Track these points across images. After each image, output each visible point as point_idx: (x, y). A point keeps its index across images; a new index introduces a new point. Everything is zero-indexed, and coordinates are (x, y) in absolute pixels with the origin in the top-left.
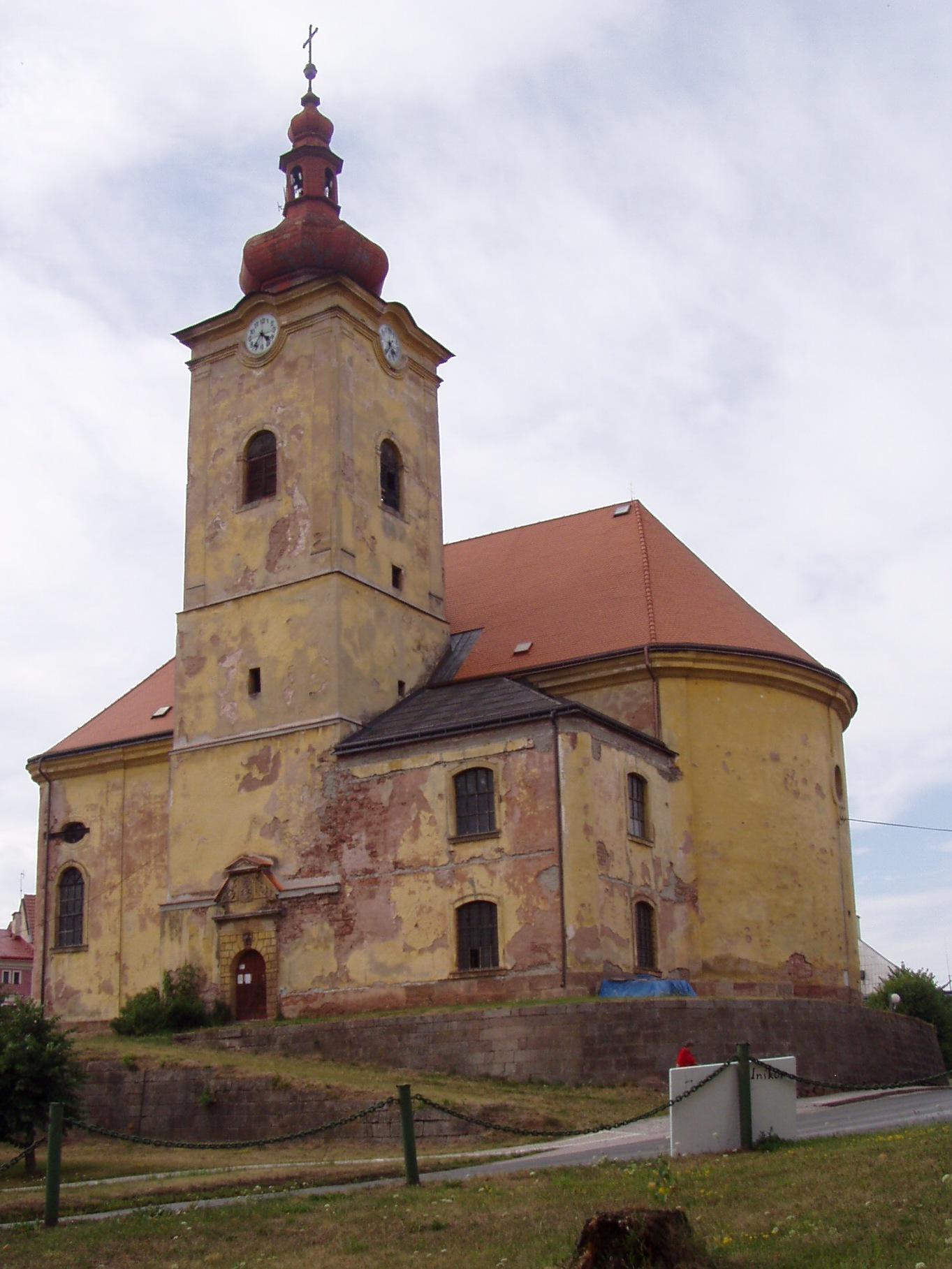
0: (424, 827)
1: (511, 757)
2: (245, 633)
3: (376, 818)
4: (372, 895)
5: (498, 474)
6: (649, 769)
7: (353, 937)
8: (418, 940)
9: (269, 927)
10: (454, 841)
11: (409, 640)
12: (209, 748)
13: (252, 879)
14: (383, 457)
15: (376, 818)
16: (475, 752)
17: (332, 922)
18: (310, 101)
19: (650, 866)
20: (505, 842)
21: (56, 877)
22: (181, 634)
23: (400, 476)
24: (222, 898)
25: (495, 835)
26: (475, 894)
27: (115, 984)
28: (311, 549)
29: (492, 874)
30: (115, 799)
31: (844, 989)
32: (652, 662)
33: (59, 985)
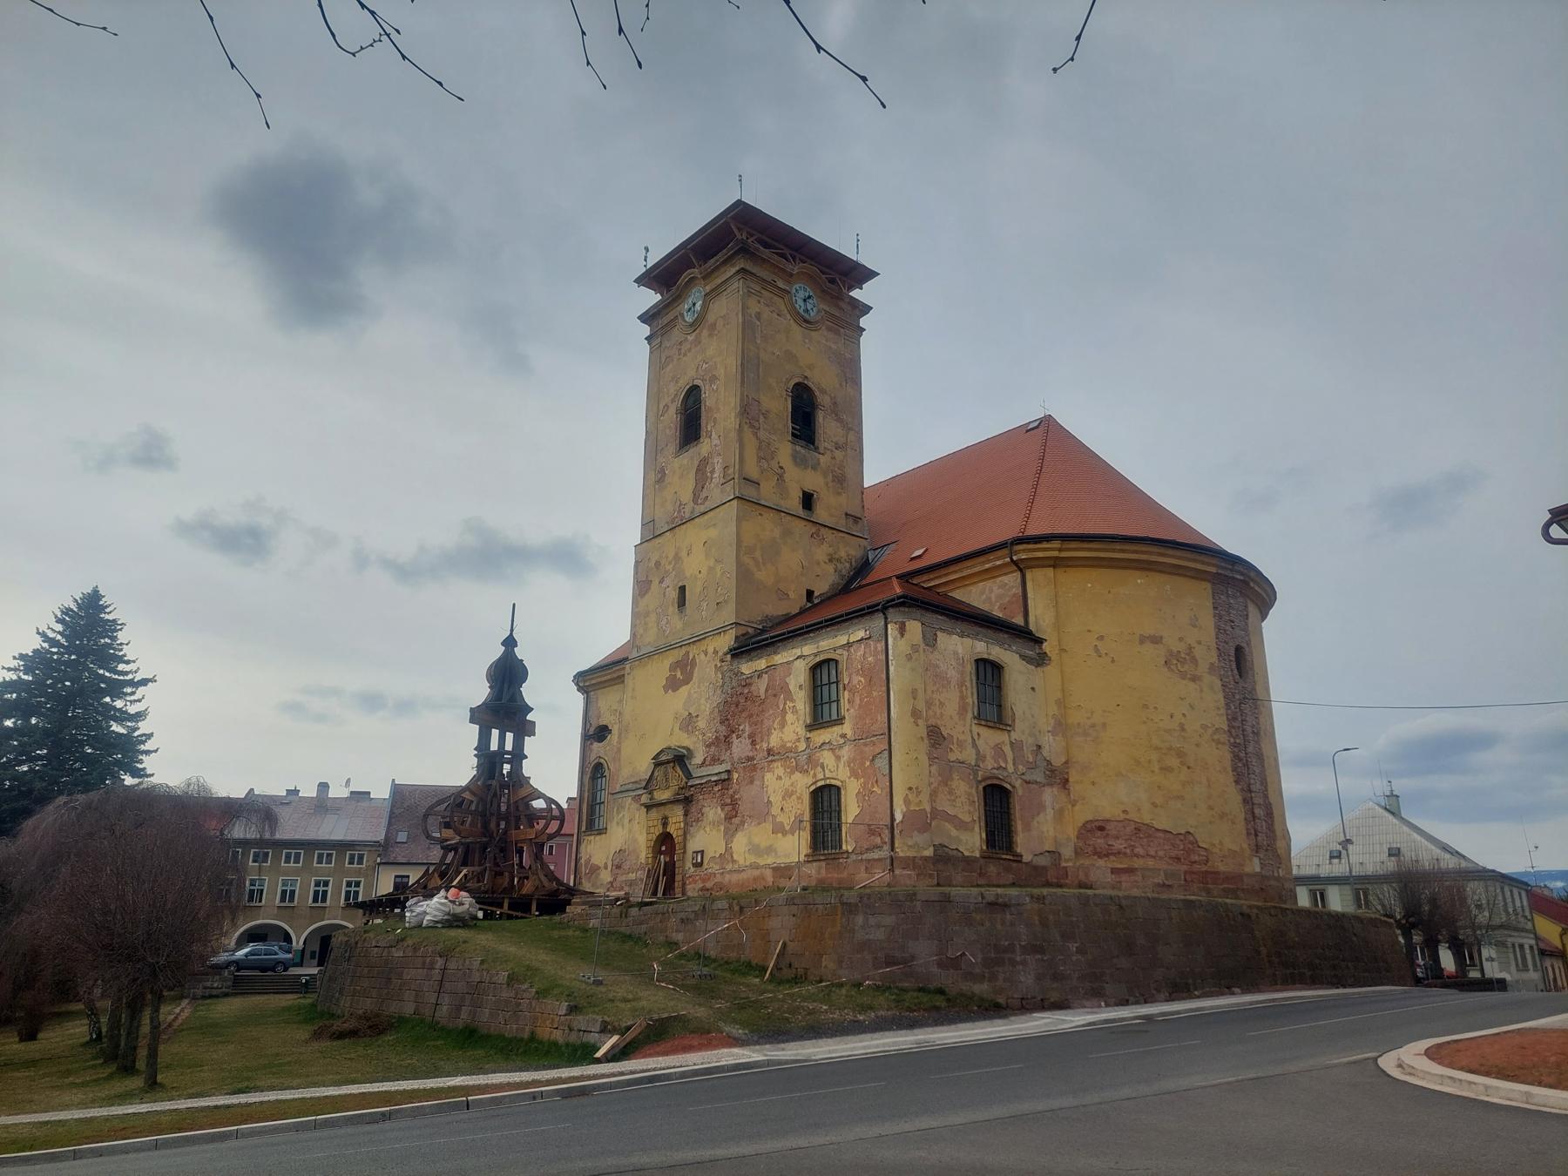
0: (790, 717)
4: (752, 782)
5: (912, 416)
6: (1008, 656)
7: (736, 821)
8: (786, 820)
10: (811, 727)
11: (821, 553)
12: (650, 655)
17: (723, 805)
19: (1007, 749)
20: (847, 728)
21: (589, 770)
22: (637, 563)
24: (649, 785)
25: (840, 721)
26: (825, 779)
29: (838, 758)
31: (1256, 875)
32: (1019, 552)
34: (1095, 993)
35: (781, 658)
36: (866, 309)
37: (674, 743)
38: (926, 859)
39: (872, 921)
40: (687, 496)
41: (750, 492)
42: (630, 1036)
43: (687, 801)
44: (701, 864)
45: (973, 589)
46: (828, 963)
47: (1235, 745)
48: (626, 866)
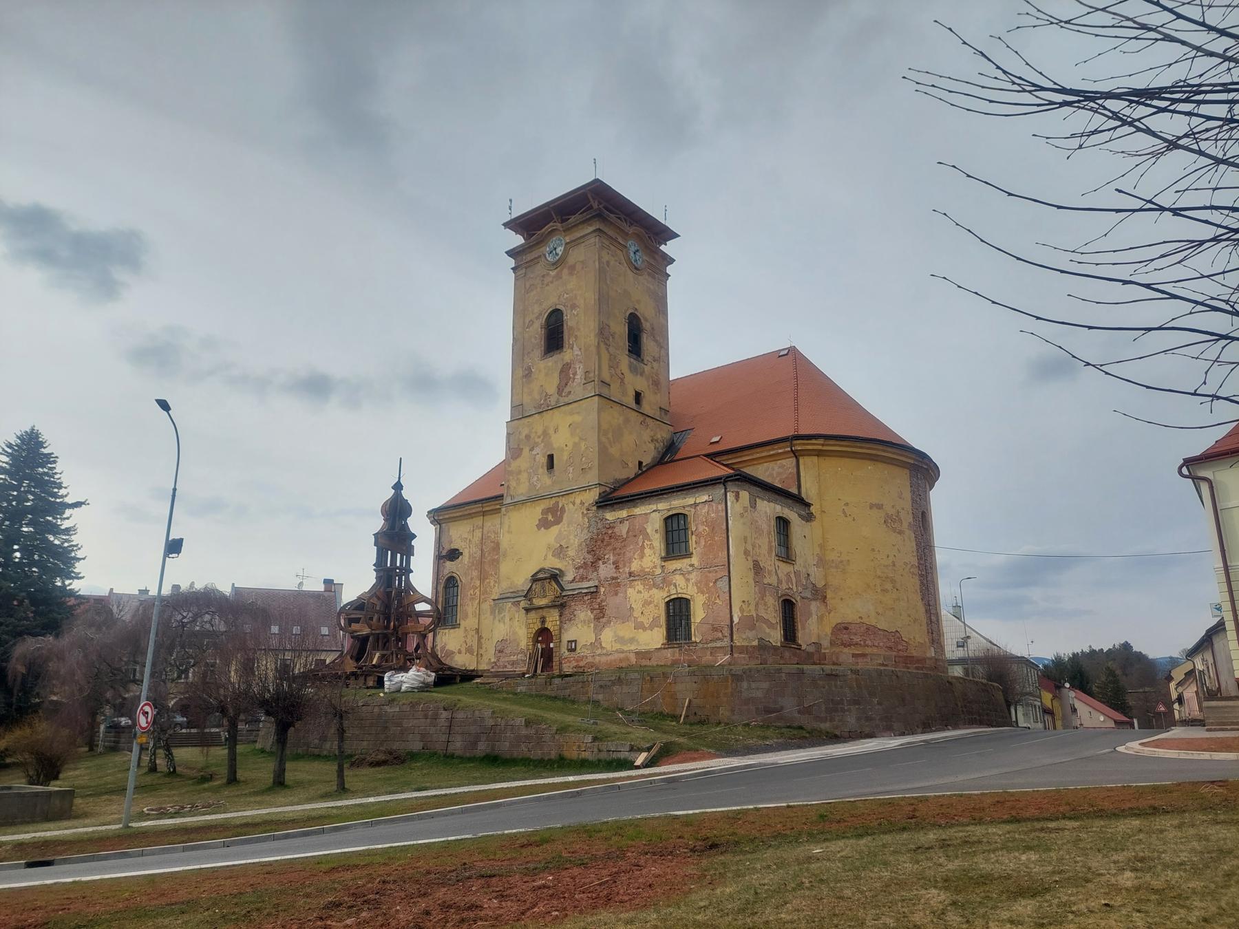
0: (647, 551)
1: (699, 507)
3: (618, 545)
5: (703, 336)
6: (791, 515)
7: (604, 620)
8: (646, 621)
10: (665, 559)
11: (646, 435)
12: (523, 502)
13: (546, 583)
14: (630, 323)
15: (618, 545)
16: (677, 503)
17: (592, 610)
19: (792, 576)
20: (695, 560)
21: (442, 582)
23: (639, 336)
24: (528, 595)
25: (689, 555)
27: (475, 648)
29: (688, 580)
30: (478, 534)
31: (931, 659)
32: (796, 444)
33: (443, 648)
34: (888, 727)
35: (640, 510)
36: (672, 261)
37: (547, 565)
38: (754, 647)
39: (753, 685)
40: (552, 389)
41: (605, 392)
42: (653, 752)
43: (562, 606)
44: (574, 650)
45: (760, 467)
46: (724, 713)
47: (921, 575)
48: (508, 651)
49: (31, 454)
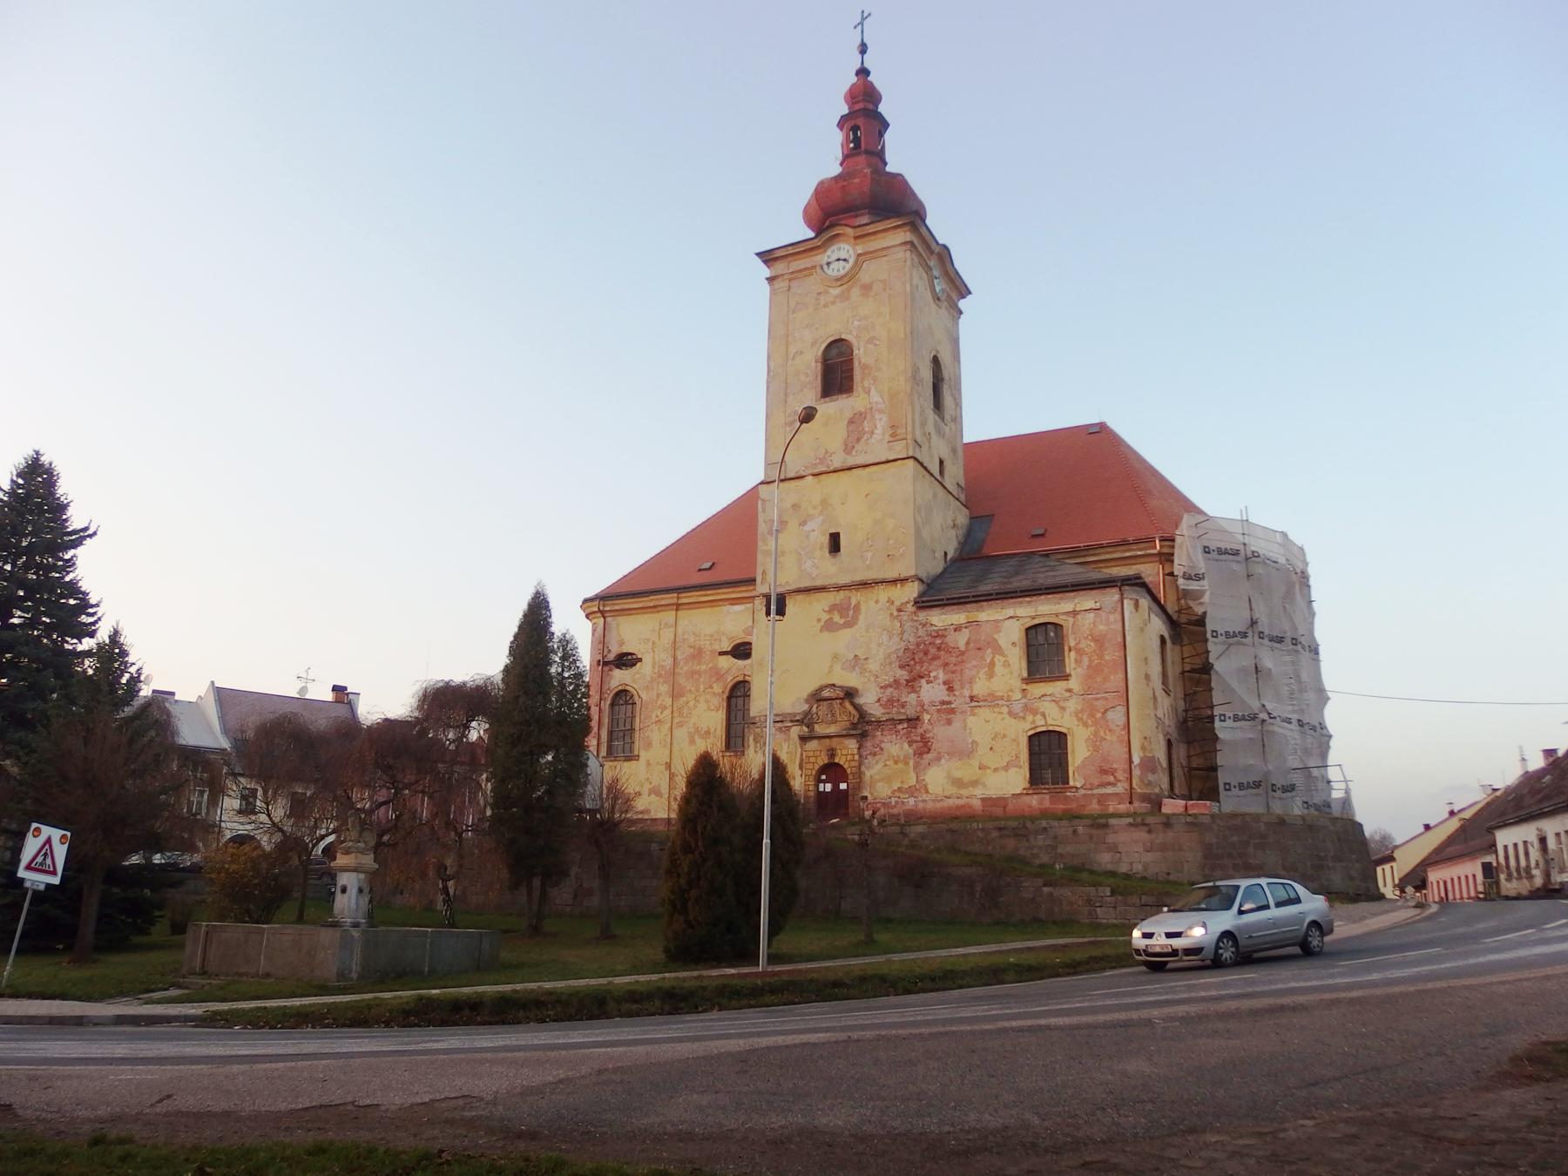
2: (825, 503)
7: (930, 756)
9: (852, 744)
17: (910, 743)
18: (863, 72)
20: (1073, 683)
24: (806, 720)
25: (1066, 677)
28: (887, 438)
29: (1063, 709)
30: (668, 635)
35: (987, 614)
43: (863, 736)
49: (37, 480)
